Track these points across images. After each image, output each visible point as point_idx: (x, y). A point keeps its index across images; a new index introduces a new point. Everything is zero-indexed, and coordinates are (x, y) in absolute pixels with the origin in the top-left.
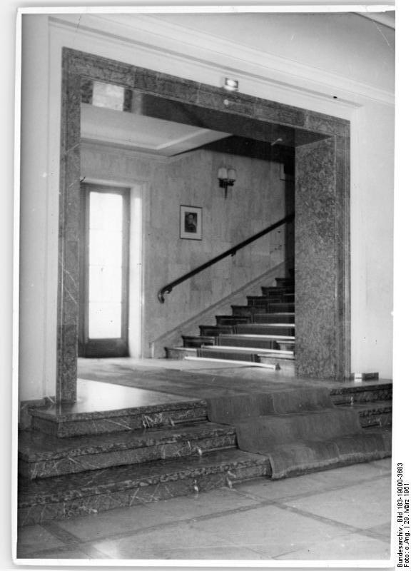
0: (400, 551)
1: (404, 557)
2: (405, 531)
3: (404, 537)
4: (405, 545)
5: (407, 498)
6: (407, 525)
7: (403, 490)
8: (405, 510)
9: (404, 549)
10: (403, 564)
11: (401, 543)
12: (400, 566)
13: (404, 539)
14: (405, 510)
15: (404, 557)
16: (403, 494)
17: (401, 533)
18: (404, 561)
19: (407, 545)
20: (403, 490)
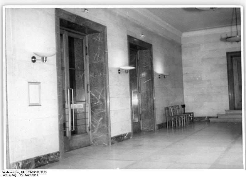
0: (9, 172)
1: (6, 174)
3: (15, 174)
9: (9, 174)
10: (3, 173)
11: (12, 173)
12: (2, 172)
13: (14, 174)
15: (6, 174)
16: (33, 174)
17: (16, 173)
18: (4, 174)
19: (11, 175)
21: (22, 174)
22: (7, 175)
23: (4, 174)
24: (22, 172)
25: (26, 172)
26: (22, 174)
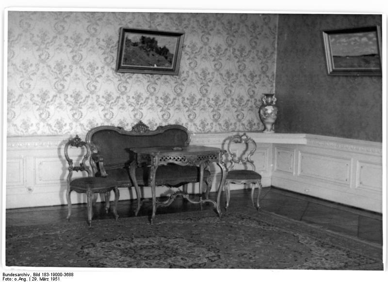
0: (14, 275)
1: (9, 277)
2: (27, 278)
3: (23, 277)
4: (18, 278)
5: (50, 279)
6: (31, 279)
8: (41, 278)
9: (15, 277)
10: (5, 276)
11: (19, 275)
12: (4, 274)
13: (22, 277)
14: (41, 278)
15: (9, 277)
16: (53, 277)
17: (26, 275)
18: (7, 277)
19: (18, 279)
21: (34, 277)
22: (10, 279)
23: (6, 277)
26: (34, 277)
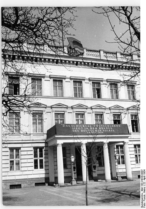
0: (142, 202)
1: (143, 204)
7: (143, 172)
10: (143, 206)
12: (142, 207)
15: (143, 204)
16: (143, 174)
17: (142, 195)
18: (143, 205)
20: (143, 172)
22: (144, 203)
24: (142, 191)
25: (142, 187)
